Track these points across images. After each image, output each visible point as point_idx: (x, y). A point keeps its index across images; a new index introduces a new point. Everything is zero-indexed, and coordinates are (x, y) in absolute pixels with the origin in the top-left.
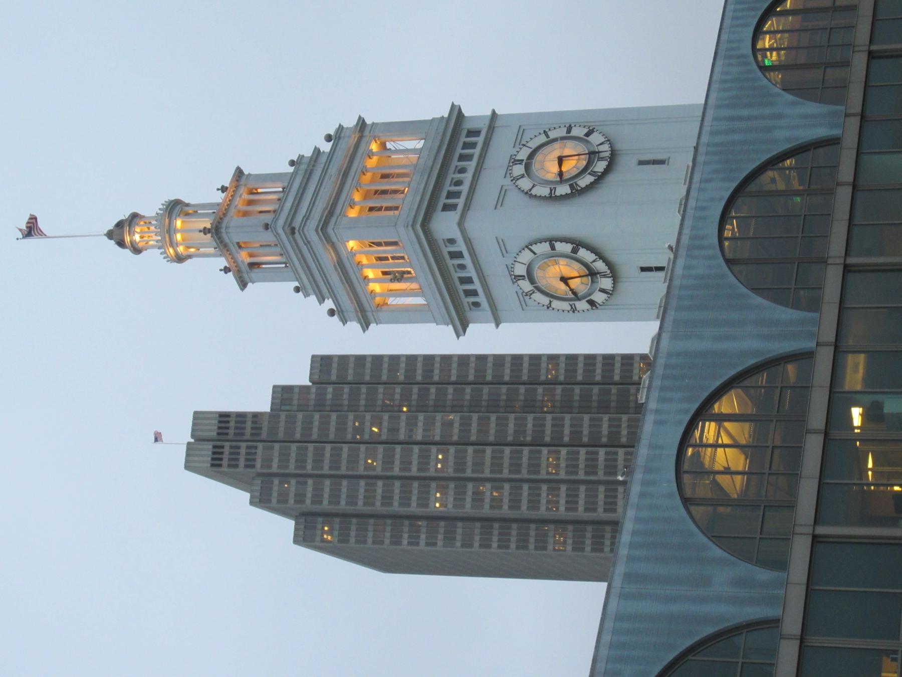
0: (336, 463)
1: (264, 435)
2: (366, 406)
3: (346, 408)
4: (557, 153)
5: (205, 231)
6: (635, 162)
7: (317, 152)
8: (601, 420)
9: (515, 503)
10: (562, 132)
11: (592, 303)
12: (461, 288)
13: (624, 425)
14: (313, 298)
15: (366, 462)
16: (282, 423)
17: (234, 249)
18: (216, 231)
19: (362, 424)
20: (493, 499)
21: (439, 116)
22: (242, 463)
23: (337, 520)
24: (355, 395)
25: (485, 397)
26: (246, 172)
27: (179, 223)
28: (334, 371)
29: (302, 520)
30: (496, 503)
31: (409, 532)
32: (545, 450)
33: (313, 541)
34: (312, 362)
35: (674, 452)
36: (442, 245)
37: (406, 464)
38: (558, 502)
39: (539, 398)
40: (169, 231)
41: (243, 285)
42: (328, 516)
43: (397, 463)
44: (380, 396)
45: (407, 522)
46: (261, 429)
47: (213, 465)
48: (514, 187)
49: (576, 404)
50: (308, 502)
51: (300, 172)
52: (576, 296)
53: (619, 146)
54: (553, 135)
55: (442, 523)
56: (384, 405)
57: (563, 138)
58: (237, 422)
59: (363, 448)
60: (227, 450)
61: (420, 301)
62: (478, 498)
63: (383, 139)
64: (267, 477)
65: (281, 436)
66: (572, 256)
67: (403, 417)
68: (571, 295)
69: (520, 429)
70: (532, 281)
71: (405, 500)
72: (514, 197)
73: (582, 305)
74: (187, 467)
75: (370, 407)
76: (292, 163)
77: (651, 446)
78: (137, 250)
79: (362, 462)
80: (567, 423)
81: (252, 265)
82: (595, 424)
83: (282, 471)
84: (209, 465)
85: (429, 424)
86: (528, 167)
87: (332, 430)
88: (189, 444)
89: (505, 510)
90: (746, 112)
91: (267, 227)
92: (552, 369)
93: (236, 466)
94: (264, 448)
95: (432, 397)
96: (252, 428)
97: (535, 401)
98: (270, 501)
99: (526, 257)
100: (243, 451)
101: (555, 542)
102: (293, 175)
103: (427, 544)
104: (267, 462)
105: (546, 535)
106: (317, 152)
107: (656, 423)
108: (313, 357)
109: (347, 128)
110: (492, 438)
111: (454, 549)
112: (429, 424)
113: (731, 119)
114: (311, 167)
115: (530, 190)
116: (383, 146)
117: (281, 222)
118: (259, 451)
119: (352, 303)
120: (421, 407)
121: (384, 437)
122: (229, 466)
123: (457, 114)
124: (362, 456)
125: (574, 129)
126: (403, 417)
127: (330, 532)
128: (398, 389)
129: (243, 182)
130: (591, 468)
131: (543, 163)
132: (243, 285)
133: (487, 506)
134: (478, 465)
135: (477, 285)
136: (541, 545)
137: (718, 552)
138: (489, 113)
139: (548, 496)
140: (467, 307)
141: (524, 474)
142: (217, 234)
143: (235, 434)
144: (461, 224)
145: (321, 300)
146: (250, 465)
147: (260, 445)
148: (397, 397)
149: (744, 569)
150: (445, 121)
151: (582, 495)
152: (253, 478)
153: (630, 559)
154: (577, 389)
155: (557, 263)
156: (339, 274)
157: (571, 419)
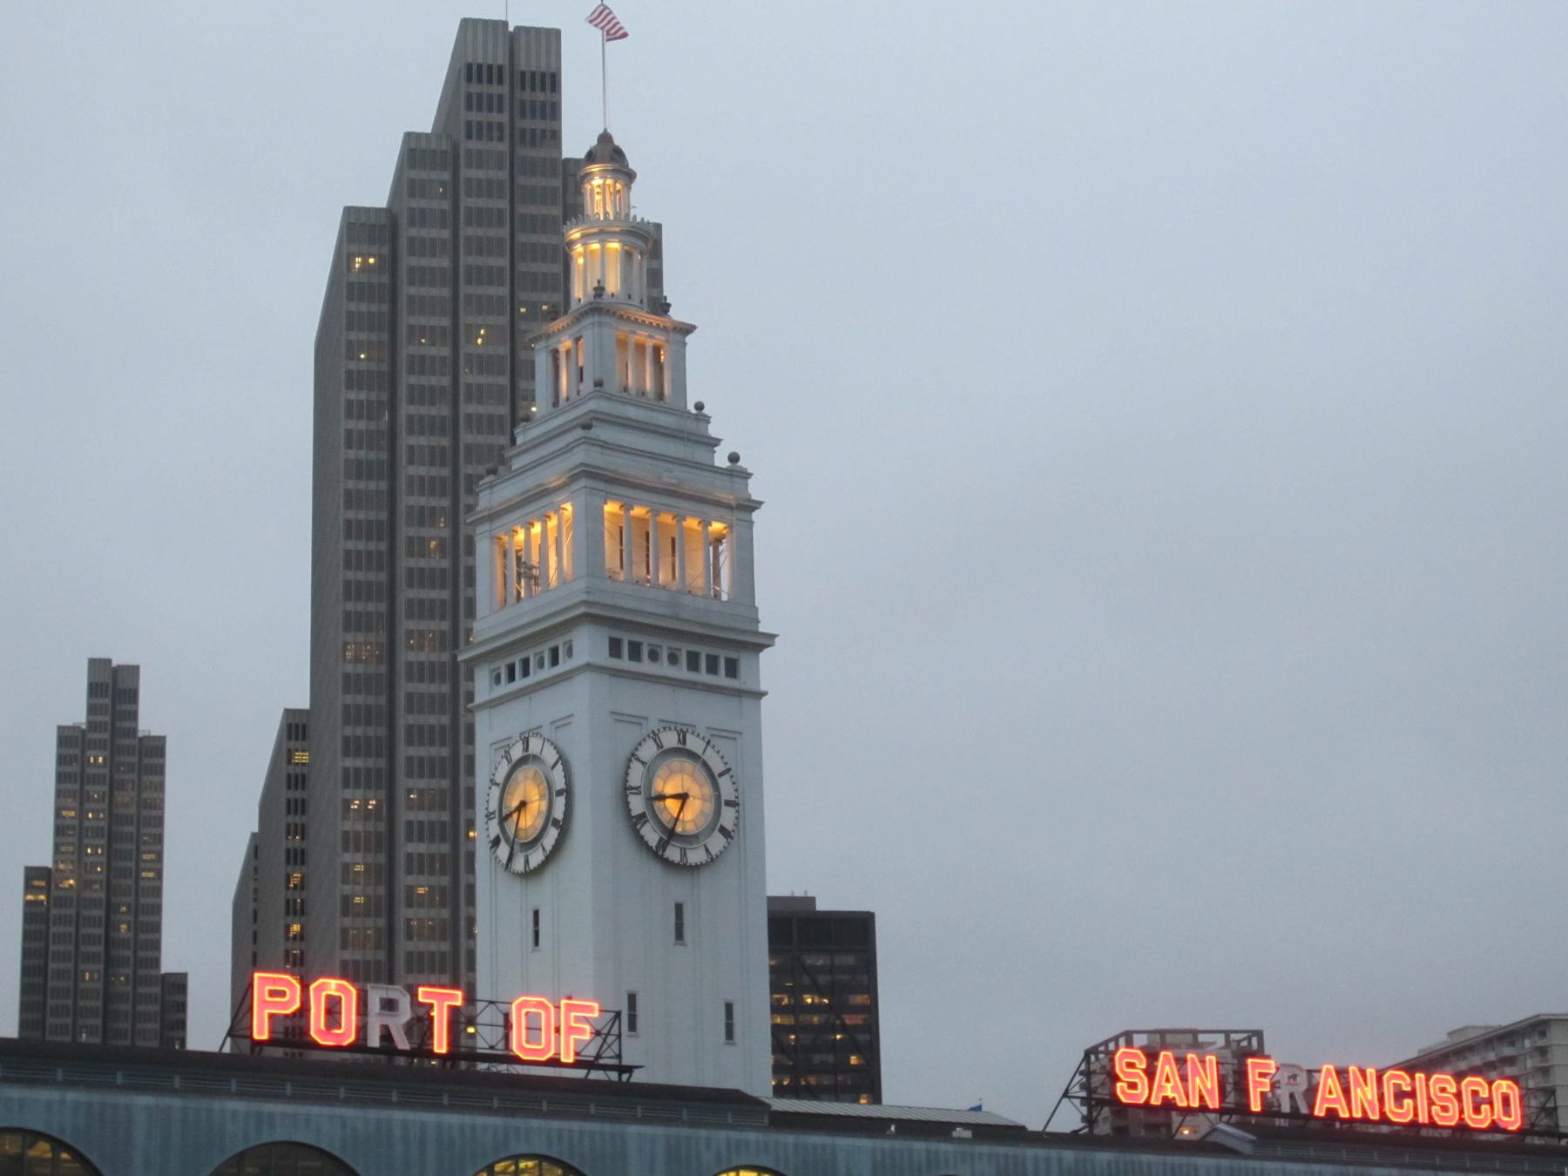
1: (523, 152)
4: (694, 790)
5: (599, 290)
6: (680, 899)
7: (714, 443)
10: (727, 792)
11: (496, 843)
12: (517, 660)
16: (541, 181)
22: (475, 116)
23: (386, 279)
27: (614, 245)
29: (384, 221)
30: (418, 547)
31: (370, 402)
35: (15, 1124)
36: (568, 638)
37: (478, 394)
38: (421, 648)
40: (602, 232)
43: (483, 379)
45: (384, 396)
46: (533, 145)
47: (469, 67)
50: (414, 232)
52: (503, 819)
53: (706, 878)
54: (724, 782)
55: (384, 456)
57: (718, 798)
58: (543, 104)
59: (504, 320)
60: (495, 89)
62: (423, 517)
65: (521, 180)
66: (549, 821)
68: (505, 812)
70: (523, 761)
72: (628, 736)
79: (480, 320)
83: (462, 187)
84: (470, 60)
87: (534, 267)
88: (505, 24)
89: (405, 562)
93: (469, 107)
96: (533, 131)
98: (413, 167)
99: (550, 756)
100: (495, 117)
103: (349, 433)
104: (478, 160)
106: (714, 443)
107: (49, 1105)
124: (491, 320)
125: (732, 810)
129: (675, 337)
131: (682, 771)
133: (412, 532)
135: (520, 682)
138: (763, 688)
139: (433, 632)
143: (523, 103)
144: (589, 667)
146: (472, 130)
151: (434, 688)
155: (542, 797)
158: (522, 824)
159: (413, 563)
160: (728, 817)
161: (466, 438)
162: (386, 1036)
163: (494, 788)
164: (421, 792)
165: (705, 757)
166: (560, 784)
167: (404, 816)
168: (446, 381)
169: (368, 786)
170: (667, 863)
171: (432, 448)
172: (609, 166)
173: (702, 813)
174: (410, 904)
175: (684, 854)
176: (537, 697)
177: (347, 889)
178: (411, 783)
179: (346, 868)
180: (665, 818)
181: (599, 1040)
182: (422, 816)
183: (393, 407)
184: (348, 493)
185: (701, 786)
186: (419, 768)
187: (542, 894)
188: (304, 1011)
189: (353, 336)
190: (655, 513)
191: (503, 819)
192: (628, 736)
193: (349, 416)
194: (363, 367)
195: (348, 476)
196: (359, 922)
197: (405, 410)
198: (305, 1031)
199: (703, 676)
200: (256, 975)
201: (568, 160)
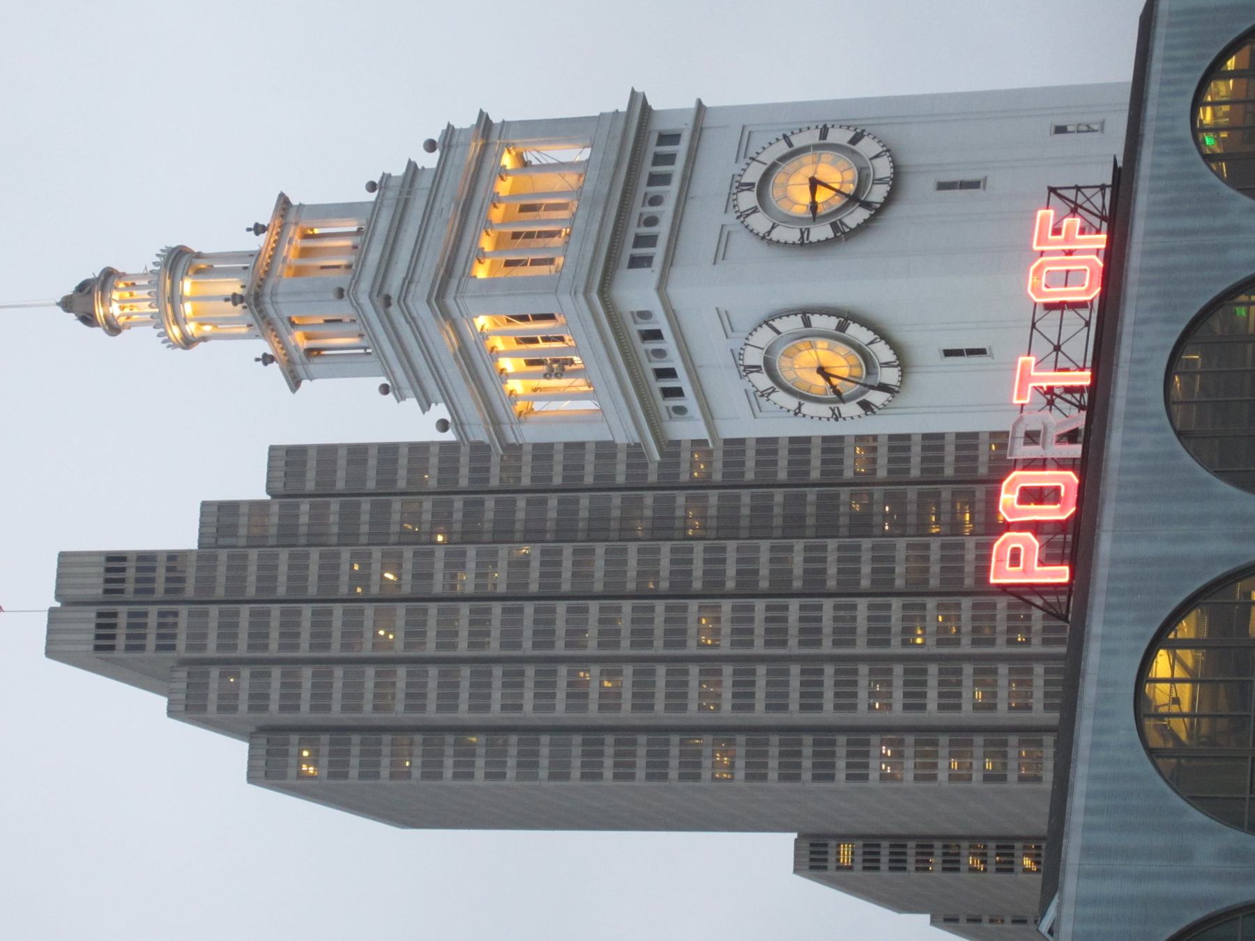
0: (321, 637)
1: (190, 591)
2: (370, 534)
3: (334, 540)
4: (807, 172)
5: (235, 299)
6: (931, 185)
7: (413, 170)
8: (790, 549)
9: (643, 700)
10: (812, 137)
11: (866, 406)
12: (658, 385)
13: (832, 557)
14: (412, 403)
15: (376, 635)
16: (222, 571)
17: (282, 328)
18: (256, 302)
19: (366, 566)
20: (604, 694)
21: (610, 109)
22: (151, 641)
23: (325, 738)
24: (349, 516)
25: (584, 514)
26: (295, 202)
28: (311, 474)
29: (262, 740)
30: (610, 700)
31: (456, 754)
32: (693, 605)
33: (283, 776)
34: (271, 458)
35: (1132, 690)
36: (629, 319)
37: (447, 636)
38: (719, 696)
39: (679, 513)
40: (172, 299)
41: (295, 382)
42: (309, 732)
44: (396, 517)
45: (450, 739)
46: (181, 580)
47: (98, 648)
48: (742, 227)
49: (745, 523)
51: (386, 203)
52: (840, 397)
53: (904, 160)
54: (798, 141)
56: (403, 532)
57: (817, 147)
58: (139, 569)
59: (369, 609)
61: (590, 405)
62: (577, 694)
63: (520, 149)
64: (197, 666)
65: (220, 592)
66: (839, 336)
67: (440, 553)
68: (831, 396)
69: (648, 569)
71: (448, 700)
72: (742, 244)
73: (850, 409)
74: (51, 653)
75: (379, 536)
76: (372, 187)
77: (1101, 683)
78: (113, 329)
79: (368, 635)
80: (731, 555)
81: (310, 352)
82: (780, 557)
84: (91, 647)
85: (486, 565)
86: (761, 196)
89: (626, 714)
90: (1189, 223)
91: (340, 293)
92: (701, 462)
93: (141, 648)
94: (190, 614)
95: (489, 515)
96: (168, 580)
97: (674, 518)
98: (203, 708)
99: (764, 337)
100: (153, 620)
101: (714, 765)
102: (377, 206)
103: (488, 776)
105: (699, 754)
106: (413, 170)
107: (1105, 652)
108: (273, 449)
109: (461, 130)
110: (598, 587)
111: (537, 783)
112: (486, 565)
113: (1171, 233)
114: (404, 196)
115: (769, 232)
116: (520, 157)
117: (365, 286)
118: (183, 621)
119: (480, 409)
120: (470, 535)
121: (406, 590)
122: (129, 648)
123: (641, 110)
124: (368, 623)
126: (440, 553)
127: (313, 761)
128: (427, 504)
129: (291, 217)
130: (776, 635)
131: (785, 186)
132: (295, 382)
133: (593, 706)
134: (575, 636)
135: (683, 381)
136: (691, 771)
137: (1198, 817)
138: (692, 105)
140: (665, 415)
141: (659, 649)
142: (257, 305)
143: (137, 591)
144: (661, 287)
145: (425, 404)
147: (183, 610)
148: (427, 517)
149: (1234, 837)
150: (621, 123)
152: (172, 669)
153: (1088, 828)
154: (746, 496)
155: (813, 347)
156: (461, 367)
157: (739, 549)
158: (844, 372)
159: (626, 705)
160: (839, 136)
161: (494, 649)
162: (1071, 437)
163: (804, 409)
164: (872, 695)
165: (769, 163)
166: (795, 323)
167: (897, 714)
168: (433, 671)
169: (866, 754)
170: (889, 200)
171: (505, 685)
172: (97, 295)
173: (833, 164)
174: (993, 707)
175: (880, 181)
176: (698, 360)
177: (977, 776)
178: (862, 706)
179: (953, 777)
180: (838, 202)
181: (1080, 210)
182: (898, 694)
183: (462, 730)
184: (552, 776)
185: (802, 166)
186: (846, 699)
187: (925, 344)
188: (1036, 527)
189: (385, 773)
190: (488, 224)
191: (840, 397)
192: (742, 244)
193: (471, 776)
194: (418, 761)
195: (535, 777)
196: (1013, 764)
197: (463, 714)
198: (1060, 526)
199: (677, 169)
200: (992, 580)
201: (201, 545)
